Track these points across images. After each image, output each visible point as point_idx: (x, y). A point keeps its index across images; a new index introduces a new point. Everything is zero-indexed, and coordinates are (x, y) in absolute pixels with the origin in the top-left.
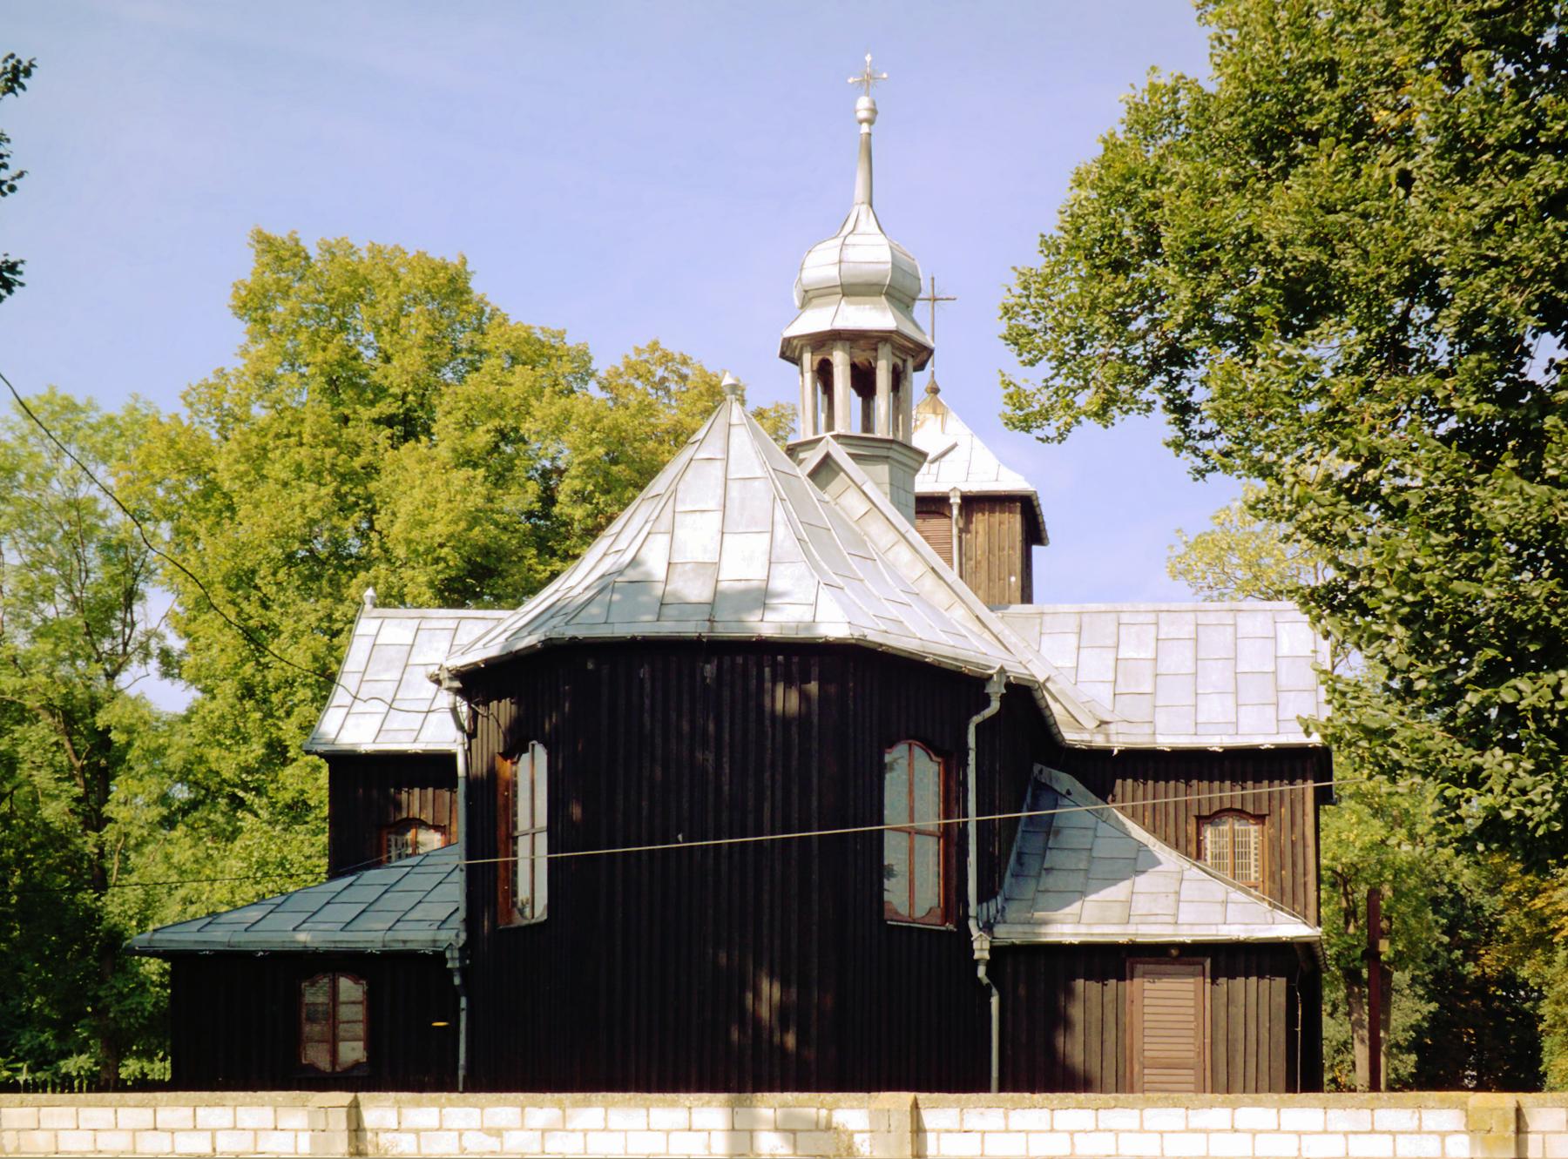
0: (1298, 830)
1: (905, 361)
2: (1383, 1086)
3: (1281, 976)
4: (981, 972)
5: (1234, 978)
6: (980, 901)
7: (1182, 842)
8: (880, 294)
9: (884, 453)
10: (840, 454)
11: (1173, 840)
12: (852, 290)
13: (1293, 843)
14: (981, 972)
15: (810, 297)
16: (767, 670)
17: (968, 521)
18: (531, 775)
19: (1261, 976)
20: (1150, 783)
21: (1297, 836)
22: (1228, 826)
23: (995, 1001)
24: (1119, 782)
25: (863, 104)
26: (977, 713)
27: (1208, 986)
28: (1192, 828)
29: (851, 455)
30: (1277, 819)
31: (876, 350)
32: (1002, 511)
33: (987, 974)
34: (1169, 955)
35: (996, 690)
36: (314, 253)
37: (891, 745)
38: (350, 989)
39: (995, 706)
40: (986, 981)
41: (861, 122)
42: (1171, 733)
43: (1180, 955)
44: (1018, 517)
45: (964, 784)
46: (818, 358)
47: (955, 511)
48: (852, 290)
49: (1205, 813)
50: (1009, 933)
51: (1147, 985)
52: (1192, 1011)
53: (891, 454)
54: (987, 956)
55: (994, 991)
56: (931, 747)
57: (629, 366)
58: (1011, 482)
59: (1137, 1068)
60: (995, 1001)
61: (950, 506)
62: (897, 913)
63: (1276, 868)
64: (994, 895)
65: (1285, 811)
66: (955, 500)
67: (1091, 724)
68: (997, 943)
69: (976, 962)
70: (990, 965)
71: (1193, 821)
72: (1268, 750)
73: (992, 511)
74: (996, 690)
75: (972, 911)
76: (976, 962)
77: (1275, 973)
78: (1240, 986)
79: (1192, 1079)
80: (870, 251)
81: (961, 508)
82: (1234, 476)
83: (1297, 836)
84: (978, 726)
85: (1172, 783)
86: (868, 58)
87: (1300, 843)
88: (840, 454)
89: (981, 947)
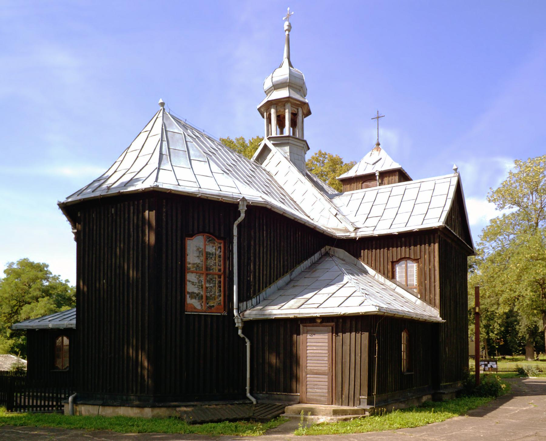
0: (432, 264)
1: (298, 109)
3: (367, 332)
4: (240, 332)
5: (345, 333)
7: (386, 272)
8: (286, 87)
9: (287, 141)
10: (270, 144)
11: (382, 272)
12: (277, 86)
13: (430, 270)
14: (240, 332)
15: (268, 92)
16: (132, 208)
17: (382, 181)
19: (356, 331)
20: (374, 250)
21: (432, 266)
22: (403, 264)
24: (362, 251)
25: (287, 23)
26: (236, 220)
27: (334, 337)
28: (390, 267)
29: (273, 144)
30: (423, 259)
31: (285, 106)
32: (392, 176)
33: (243, 333)
34: (316, 322)
35: (243, 209)
36: (235, 141)
37: (192, 235)
39: (243, 215)
40: (242, 336)
41: (286, 31)
42: (383, 229)
43: (321, 322)
44: (397, 177)
45: (232, 251)
46: (268, 113)
47: (378, 178)
48: (277, 86)
49: (395, 260)
51: (309, 336)
52: (327, 348)
53: (290, 141)
55: (247, 340)
57: (313, 158)
58: (396, 166)
59: (304, 374)
61: (376, 176)
62: (195, 308)
63: (423, 280)
65: (427, 256)
66: (377, 174)
67: (351, 229)
68: (245, 319)
69: (237, 328)
71: (390, 264)
72: (416, 231)
73: (389, 176)
74: (243, 209)
76: (237, 328)
77: (363, 330)
78: (350, 338)
79: (326, 380)
80: (282, 73)
81: (380, 176)
83: (432, 266)
84: (239, 226)
85: (382, 250)
86: (288, 9)
87: (433, 269)
88: (270, 144)
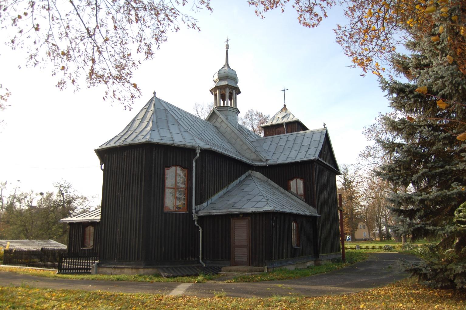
2: (241, 254)
4: (196, 223)
6: (196, 204)
9: (226, 109)
18: (339, 206)
23: (201, 231)
33: (198, 223)
35: (198, 151)
37: (169, 167)
38: (92, 229)
39: (198, 155)
40: (197, 225)
50: (202, 213)
53: (228, 109)
54: (196, 219)
55: (200, 228)
56: (183, 167)
60: (201, 231)
62: (170, 209)
64: (202, 203)
70: (198, 221)
74: (198, 151)
75: (193, 207)
76: (194, 221)
82: (151, 45)
89: (195, 217)
